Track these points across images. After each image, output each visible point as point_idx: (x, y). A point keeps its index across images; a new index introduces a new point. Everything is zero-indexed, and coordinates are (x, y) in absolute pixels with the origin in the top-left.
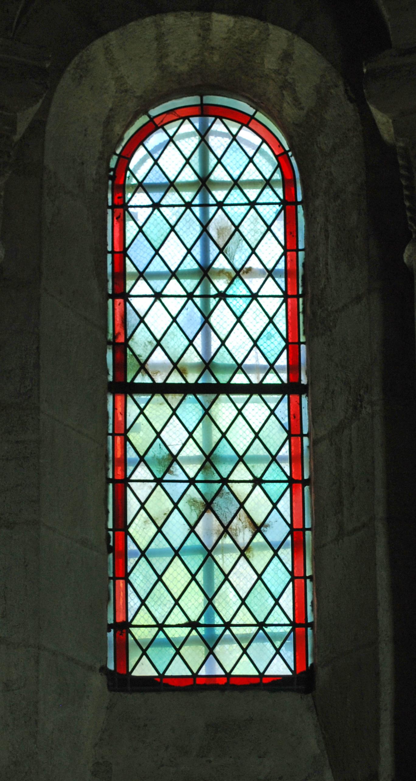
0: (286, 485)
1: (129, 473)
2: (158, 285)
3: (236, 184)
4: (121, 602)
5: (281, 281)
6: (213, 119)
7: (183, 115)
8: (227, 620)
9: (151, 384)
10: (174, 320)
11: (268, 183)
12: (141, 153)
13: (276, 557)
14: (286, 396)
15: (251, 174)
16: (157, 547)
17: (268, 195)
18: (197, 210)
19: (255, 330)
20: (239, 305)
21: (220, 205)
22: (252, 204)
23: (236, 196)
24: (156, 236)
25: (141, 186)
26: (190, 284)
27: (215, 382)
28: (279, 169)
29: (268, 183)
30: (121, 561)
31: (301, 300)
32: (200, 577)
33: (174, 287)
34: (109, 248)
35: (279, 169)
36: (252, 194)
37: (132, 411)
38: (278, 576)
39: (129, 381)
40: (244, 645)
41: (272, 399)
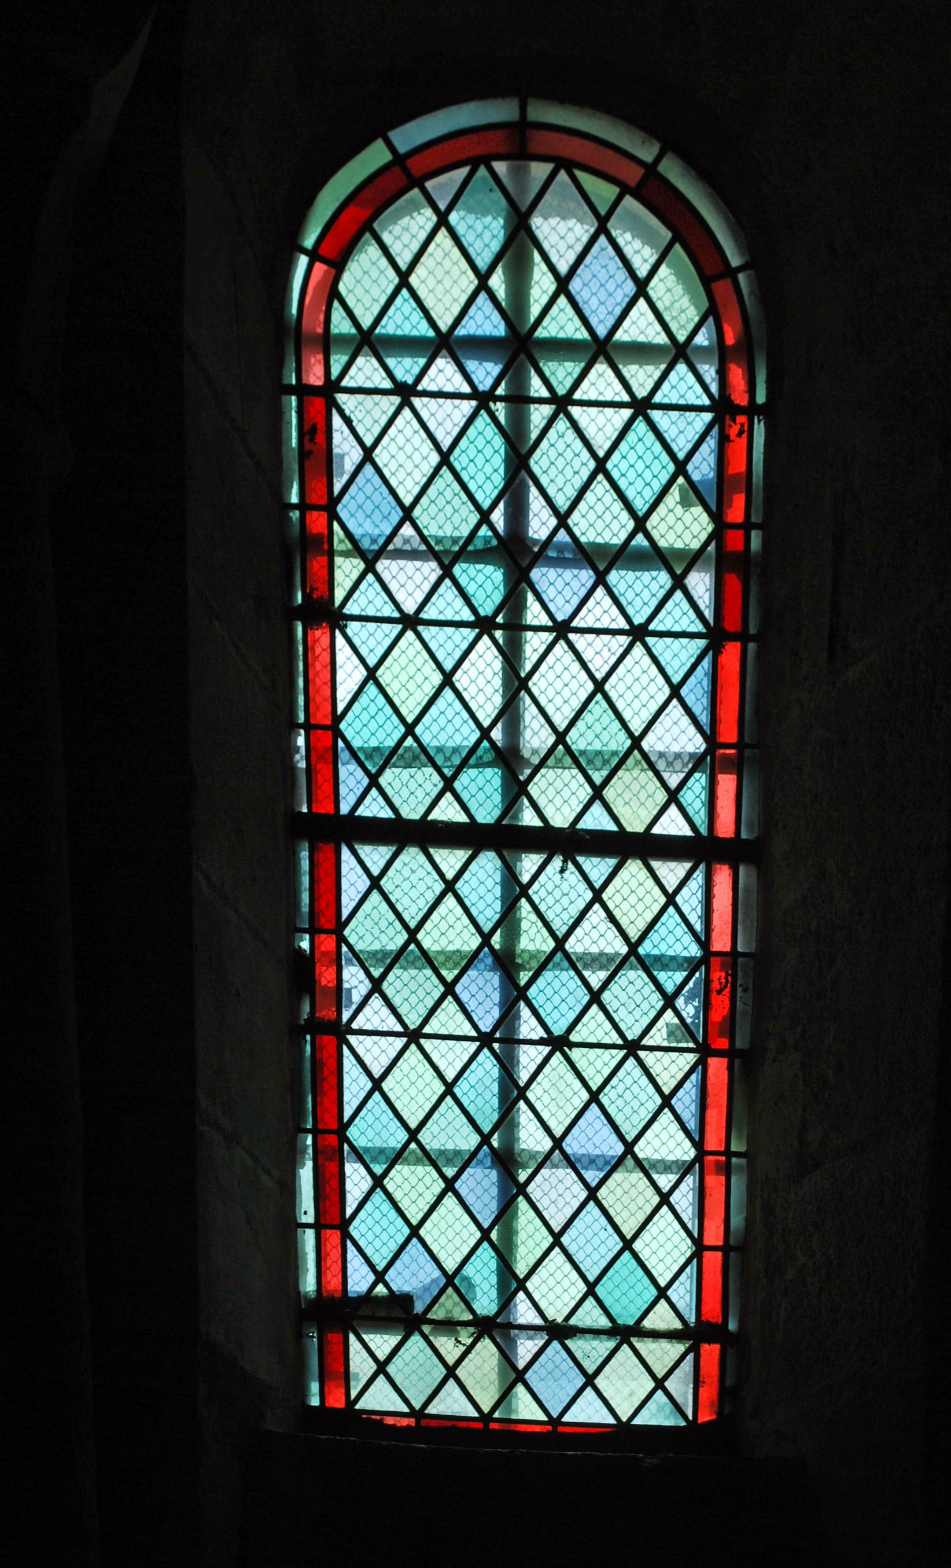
0: (708, 417)
1: (335, 372)
2: (405, 368)
3: (601, 349)
4: (320, 665)
5: (709, 372)
6: (548, 167)
7: (469, 152)
8: (560, 617)
9: (389, 820)
10: (449, 1089)
11: (680, 352)
12: (368, 256)
13: (670, 891)
14: (702, 867)
15: (642, 326)
16: (399, 359)
17: (682, 386)
18: (500, 409)
19: (632, 691)
20: (600, 652)
21: (562, 403)
22: (641, 407)
23: (601, 383)
24: (403, 452)
25: (368, 341)
26: (485, 372)
27: (537, 823)
28: (711, 319)
29: (680, 352)
30: (333, 1167)
31: (752, 646)
32: (494, 1235)
33: (444, 374)
34: (301, 718)
35: (711, 319)
36: (642, 377)
37: (353, 882)
38: (667, 1247)
39: (345, 809)
40: (598, 778)
41: (671, 872)
